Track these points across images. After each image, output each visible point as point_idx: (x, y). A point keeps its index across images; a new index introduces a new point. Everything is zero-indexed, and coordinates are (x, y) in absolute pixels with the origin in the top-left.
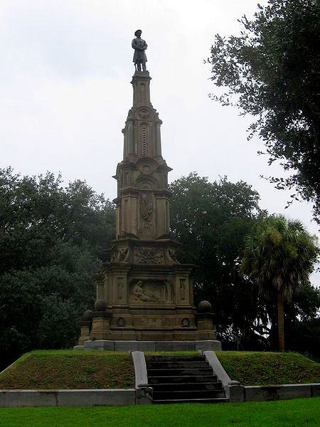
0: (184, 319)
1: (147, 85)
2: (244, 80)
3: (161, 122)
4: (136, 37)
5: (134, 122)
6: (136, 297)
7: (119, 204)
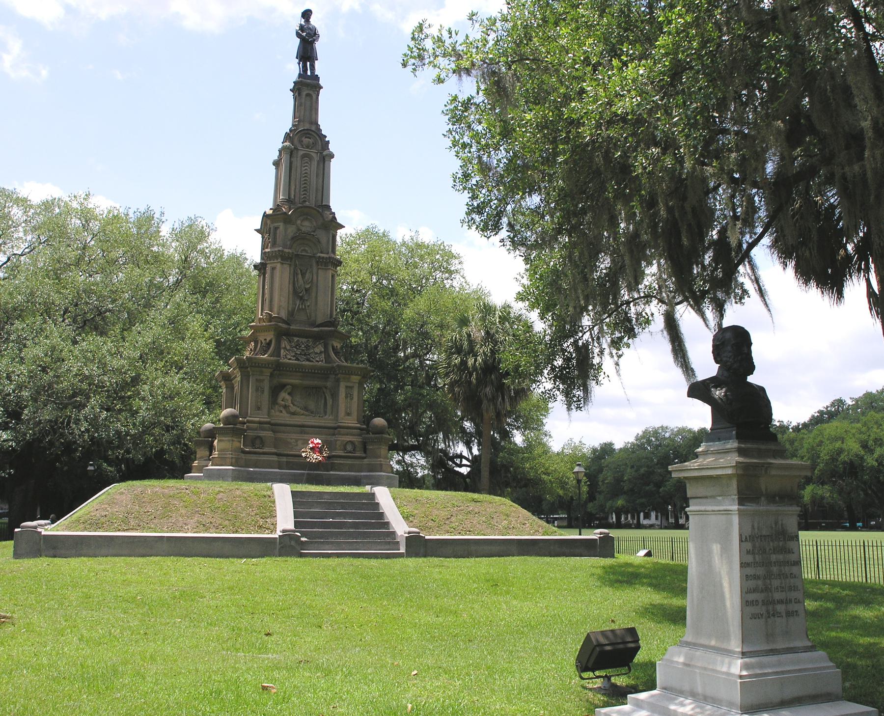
1: (314, 97)
6: (281, 409)
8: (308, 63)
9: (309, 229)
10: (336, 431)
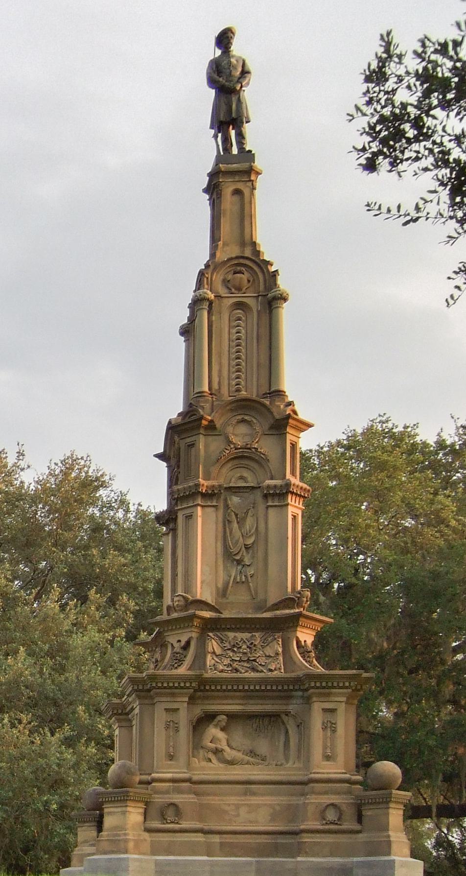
2: (99, 693)
4: (219, 52)
7: (171, 526)
8: (233, 133)
10: (307, 788)
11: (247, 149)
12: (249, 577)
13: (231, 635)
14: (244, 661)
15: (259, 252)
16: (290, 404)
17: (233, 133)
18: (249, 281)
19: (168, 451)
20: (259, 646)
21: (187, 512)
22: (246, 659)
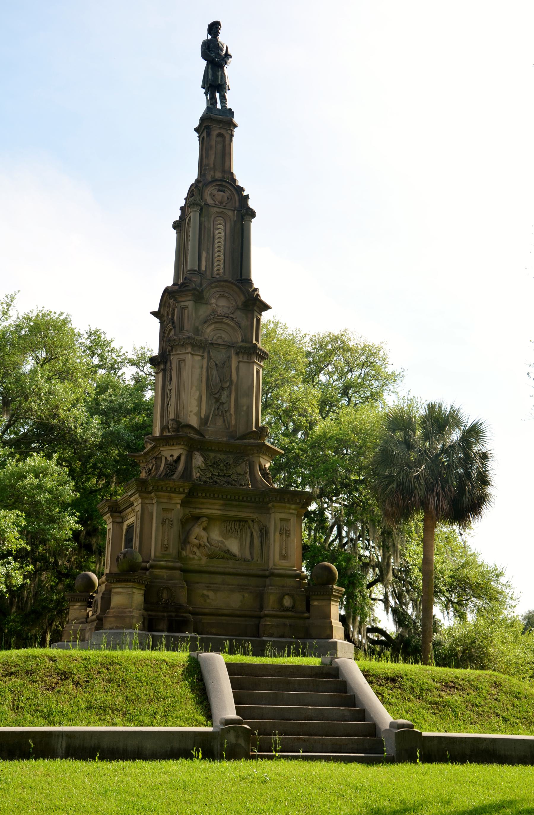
0: (164, 588)
1: (227, 137)
3: (253, 214)
5: (201, 210)
6: (195, 549)
7: (162, 367)
8: (218, 95)
9: (226, 310)
10: (268, 581)
11: (228, 108)
12: (224, 412)
13: (212, 455)
14: (221, 476)
15: (235, 180)
16: (256, 290)
17: (218, 95)
18: (228, 198)
19: (162, 310)
20: (232, 466)
21: (182, 357)
22: (223, 475)
